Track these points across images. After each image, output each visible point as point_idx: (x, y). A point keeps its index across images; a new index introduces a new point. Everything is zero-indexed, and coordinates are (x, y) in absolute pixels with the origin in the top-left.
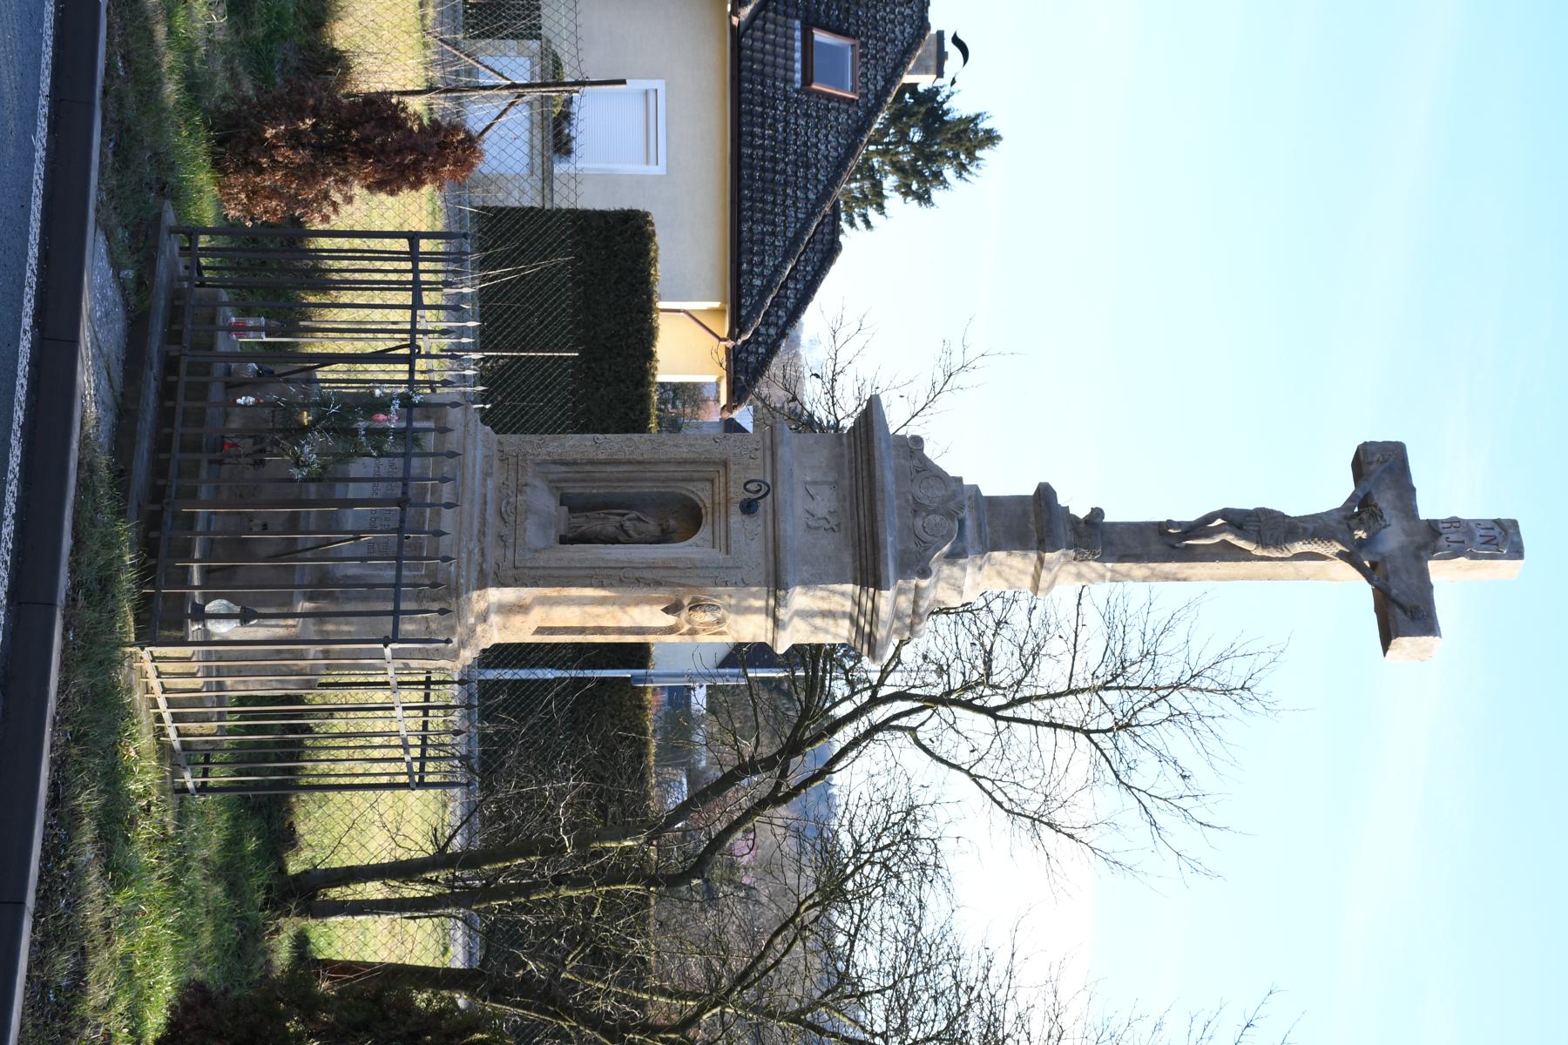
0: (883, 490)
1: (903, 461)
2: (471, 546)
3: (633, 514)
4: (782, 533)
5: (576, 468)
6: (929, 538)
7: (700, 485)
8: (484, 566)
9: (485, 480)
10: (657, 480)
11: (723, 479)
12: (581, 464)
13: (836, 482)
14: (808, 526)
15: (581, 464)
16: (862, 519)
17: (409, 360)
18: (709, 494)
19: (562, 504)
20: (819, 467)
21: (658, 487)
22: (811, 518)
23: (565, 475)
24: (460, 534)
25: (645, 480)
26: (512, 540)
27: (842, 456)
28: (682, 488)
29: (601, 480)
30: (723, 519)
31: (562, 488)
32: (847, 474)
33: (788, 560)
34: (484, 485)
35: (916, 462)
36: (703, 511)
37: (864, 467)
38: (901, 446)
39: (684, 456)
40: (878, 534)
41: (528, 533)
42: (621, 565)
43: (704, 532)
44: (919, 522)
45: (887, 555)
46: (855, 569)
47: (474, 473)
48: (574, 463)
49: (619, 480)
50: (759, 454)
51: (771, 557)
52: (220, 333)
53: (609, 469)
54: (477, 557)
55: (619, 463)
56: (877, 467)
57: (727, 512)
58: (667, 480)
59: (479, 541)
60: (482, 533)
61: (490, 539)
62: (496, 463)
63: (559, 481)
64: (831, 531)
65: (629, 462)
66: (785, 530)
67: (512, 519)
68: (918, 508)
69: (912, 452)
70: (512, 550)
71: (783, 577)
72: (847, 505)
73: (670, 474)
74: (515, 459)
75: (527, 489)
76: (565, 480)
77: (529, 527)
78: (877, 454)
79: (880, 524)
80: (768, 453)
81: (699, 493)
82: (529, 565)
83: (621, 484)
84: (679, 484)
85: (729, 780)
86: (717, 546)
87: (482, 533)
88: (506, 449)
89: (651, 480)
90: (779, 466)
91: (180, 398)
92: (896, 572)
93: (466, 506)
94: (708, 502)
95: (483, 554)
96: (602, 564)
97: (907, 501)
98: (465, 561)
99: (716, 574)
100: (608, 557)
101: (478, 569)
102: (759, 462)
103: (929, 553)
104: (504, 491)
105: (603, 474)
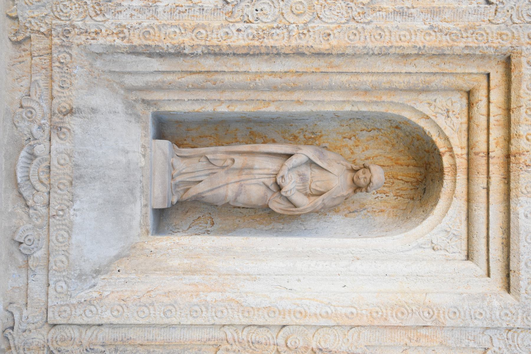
7: (442, 101)
10: (356, 90)
11: (497, 96)
12: (193, 55)
15: (193, 55)
21: (354, 103)
23: (159, 78)
25: (330, 88)
26: (39, 254)
28: (403, 106)
29: (232, 88)
36: (446, 161)
39: (420, 41)
49: (275, 88)
57: (507, 179)
58: (374, 89)
63: (147, 89)
65: (299, 53)
67: (40, 198)
70: (41, 276)
73: (384, 79)
75: (73, 122)
76: (159, 88)
81: (441, 121)
82: (79, 321)
83: (277, 96)
84: (396, 99)
85: (232, 22)
89: (341, 88)
96: (240, 319)
99: (484, 340)
105: (241, 78)
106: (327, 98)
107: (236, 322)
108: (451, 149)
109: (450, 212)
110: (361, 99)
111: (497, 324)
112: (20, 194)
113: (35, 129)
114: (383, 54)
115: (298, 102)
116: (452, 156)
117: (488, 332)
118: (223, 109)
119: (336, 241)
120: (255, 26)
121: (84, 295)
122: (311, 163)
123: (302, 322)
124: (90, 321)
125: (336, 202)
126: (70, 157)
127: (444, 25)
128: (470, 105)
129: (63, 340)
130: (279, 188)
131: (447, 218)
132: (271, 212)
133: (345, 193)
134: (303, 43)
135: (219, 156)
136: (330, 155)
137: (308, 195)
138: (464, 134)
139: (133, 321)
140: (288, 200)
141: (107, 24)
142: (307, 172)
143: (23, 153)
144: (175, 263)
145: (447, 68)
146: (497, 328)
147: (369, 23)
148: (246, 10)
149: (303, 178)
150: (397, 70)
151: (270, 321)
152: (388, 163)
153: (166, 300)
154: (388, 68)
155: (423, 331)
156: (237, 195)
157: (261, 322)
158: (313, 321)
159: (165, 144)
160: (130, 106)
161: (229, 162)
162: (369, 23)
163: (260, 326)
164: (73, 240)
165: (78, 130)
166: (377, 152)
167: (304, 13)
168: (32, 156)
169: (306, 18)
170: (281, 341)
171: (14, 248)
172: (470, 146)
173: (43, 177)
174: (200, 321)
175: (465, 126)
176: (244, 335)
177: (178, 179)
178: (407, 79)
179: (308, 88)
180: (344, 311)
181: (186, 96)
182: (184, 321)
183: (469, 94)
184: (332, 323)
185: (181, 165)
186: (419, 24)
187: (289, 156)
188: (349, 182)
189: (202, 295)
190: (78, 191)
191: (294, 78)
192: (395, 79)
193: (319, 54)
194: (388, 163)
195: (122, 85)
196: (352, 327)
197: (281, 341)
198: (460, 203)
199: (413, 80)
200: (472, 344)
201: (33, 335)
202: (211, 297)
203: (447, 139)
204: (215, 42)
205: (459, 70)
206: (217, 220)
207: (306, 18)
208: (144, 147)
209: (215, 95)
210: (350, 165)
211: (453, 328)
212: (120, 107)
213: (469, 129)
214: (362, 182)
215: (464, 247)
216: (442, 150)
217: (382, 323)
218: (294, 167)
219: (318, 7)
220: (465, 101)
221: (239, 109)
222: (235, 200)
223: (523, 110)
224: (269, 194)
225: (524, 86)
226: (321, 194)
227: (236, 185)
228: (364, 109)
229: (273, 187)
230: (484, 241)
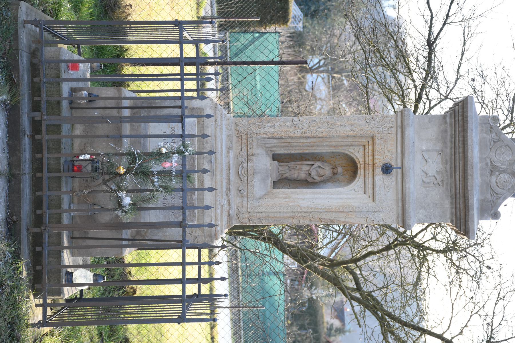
0: (472, 168)
1: (485, 135)
2: (223, 202)
3: (318, 164)
4: (407, 190)
5: (283, 141)
6: (499, 190)
7: (357, 148)
8: (231, 212)
9: (228, 152)
10: (332, 146)
11: (371, 147)
13: (442, 151)
14: (423, 181)
16: (458, 182)
17: (181, 119)
18: (362, 154)
19: (274, 160)
20: (431, 140)
21: (331, 150)
22: (425, 175)
24: (216, 197)
25: (324, 146)
26: (245, 193)
27: (446, 131)
28: (346, 150)
29: (296, 146)
30: (371, 176)
31: (274, 151)
32: (449, 144)
33: (411, 208)
34: (228, 157)
35: (493, 135)
36: (359, 165)
37: (461, 146)
38: (485, 124)
39: (348, 133)
40: (468, 199)
41: (255, 189)
42: (310, 210)
43: (359, 181)
44: (494, 179)
45: (473, 214)
46: (452, 213)
47: (222, 151)
48: (281, 138)
49: (308, 146)
50: (394, 130)
51: (400, 204)
52: (65, 251)
53: (302, 141)
54: (226, 207)
55: (307, 137)
56: (469, 150)
59: (227, 195)
60: (229, 190)
61: (233, 192)
62: (234, 139)
63: (272, 147)
64: (437, 185)
66: (409, 189)
67: (245, 178)
68: (493, 169)
69: (491, 128)
70: (246, 199)
71: (408, 221)
72: (448, 167)
74: (246, 136)
75: (254, 158)
77: (255, 184)
78: (469, 141)
79: (470, 192)
80: (399, 130)
82: (256, 211)
83: (308, 148)
84: (343, 148)
86: (367, 193)
87: (229, 190)
88: (240, 129)
90: (406, 142)
91: (45, 151)
92: (478, 217)
93: (219, 189)
94: (361, 160)
95: (229, 204)
97: (487, 164)
98: (219, 214)
99: (367, 215)
100: (302, 205)
101: (227, 214)
102: (393, 136)
103: (499, 201)
104: (240, 159)
106: (323, 148)
107: (299, 211)
108: (359, 162)
109: (360, 180)
110: (333, 148)
111: (370, 210)
112: (240, 178)
113: (243, 160)
114: (338, 137)
115: (315, 149)
116: (360, 164)
117: (368, 213)
118: (293, 152)
119: (327, 189)
120: (302, 130)
121: (257, 204)
122: (319, 167)
123: (316, 211)
124: (259, 211)
125: (328, 178)
126: (253, 167)
127: (355, 129)
128: (364, 149)
129: (252, 216)
130: (310, 174)
131: (358, 182)
132: (308, 182)
133: (331, 176)
134: (315, 135)
135: (292, 165)
136: (326, 164)
137: (319, 176)
138: (363, 158)
139: (271, 211)
140: (313, 178)
141: (262, 131)
142: (319, 169)
143: (240, 167)
144: (281, 196)
145: (357, 140)
146: (370, 212)
147: (334, 128)
148: (300, 126)
149: (317, 171)
150: (342, 140)
151: (308, 211)
152: (346, 165)
153: (279, 205)
154: (340, 140)
155: (350, 213)
156: (298, 176)
157: (305, 211)
158: (319, 210)
159: (276, 162)
160: (267, 152)
161: (295, 167)
162: (334, 128)
163: (305, 212)
164: (254, 190)
165: (254, 160)
166: (342, 162)
167: (315, 126)
168: (243, 167)
169: (316, 127)
170: (311, 216)
171: (238, 192)
172: (365, 161)
173: (246, 173)
174: (289, 211)
175: (363, 156)
176: (301, 214)
177: (280, 172)
178: (345, 143)
179: (318, 146)
180: (328, 207)
181: (283, 149)
182: (284, 211)
183: (364, 146)
184: (325, 211)
185: (280, 168)
186: (348, 129)
187: (313, 165)
188: (332, 172)
189: (289, 204)
190: (255, 176)
191: (313, 143)
192: (342, 143)
193: (320, 137)
194: (346, 165)
195: (265, 146)
196: (330, 212)
197: (311, 216)
198: (362, 178)
199: (347, 143)
200: (363, 216)
201: (244, 215)
202: (291, 204)
203: (358, 159)
204: (291, 135)
205: (360, 140)
206: (291, 185)
207: (316, 127)
208: (270, 163)
209: (291, 148)
210: (332, 167)
211: (358, 212)
212: (264, 152)
213: (364, 156)
214: (335, 172)
215: (364, 190)
216: (357, 162)
217: (338, 211)
218: (314, 168)
219: (319, 125)
220: (363, 148)
221: (297, 152)
222: (297, 178)
223: (376, 152)
224: (307, 176)
225: (377, 145)
226: (323, 176)
227: (297, 174)
228: (334, 151)
229: (308, 174)
230: (368, 188)
